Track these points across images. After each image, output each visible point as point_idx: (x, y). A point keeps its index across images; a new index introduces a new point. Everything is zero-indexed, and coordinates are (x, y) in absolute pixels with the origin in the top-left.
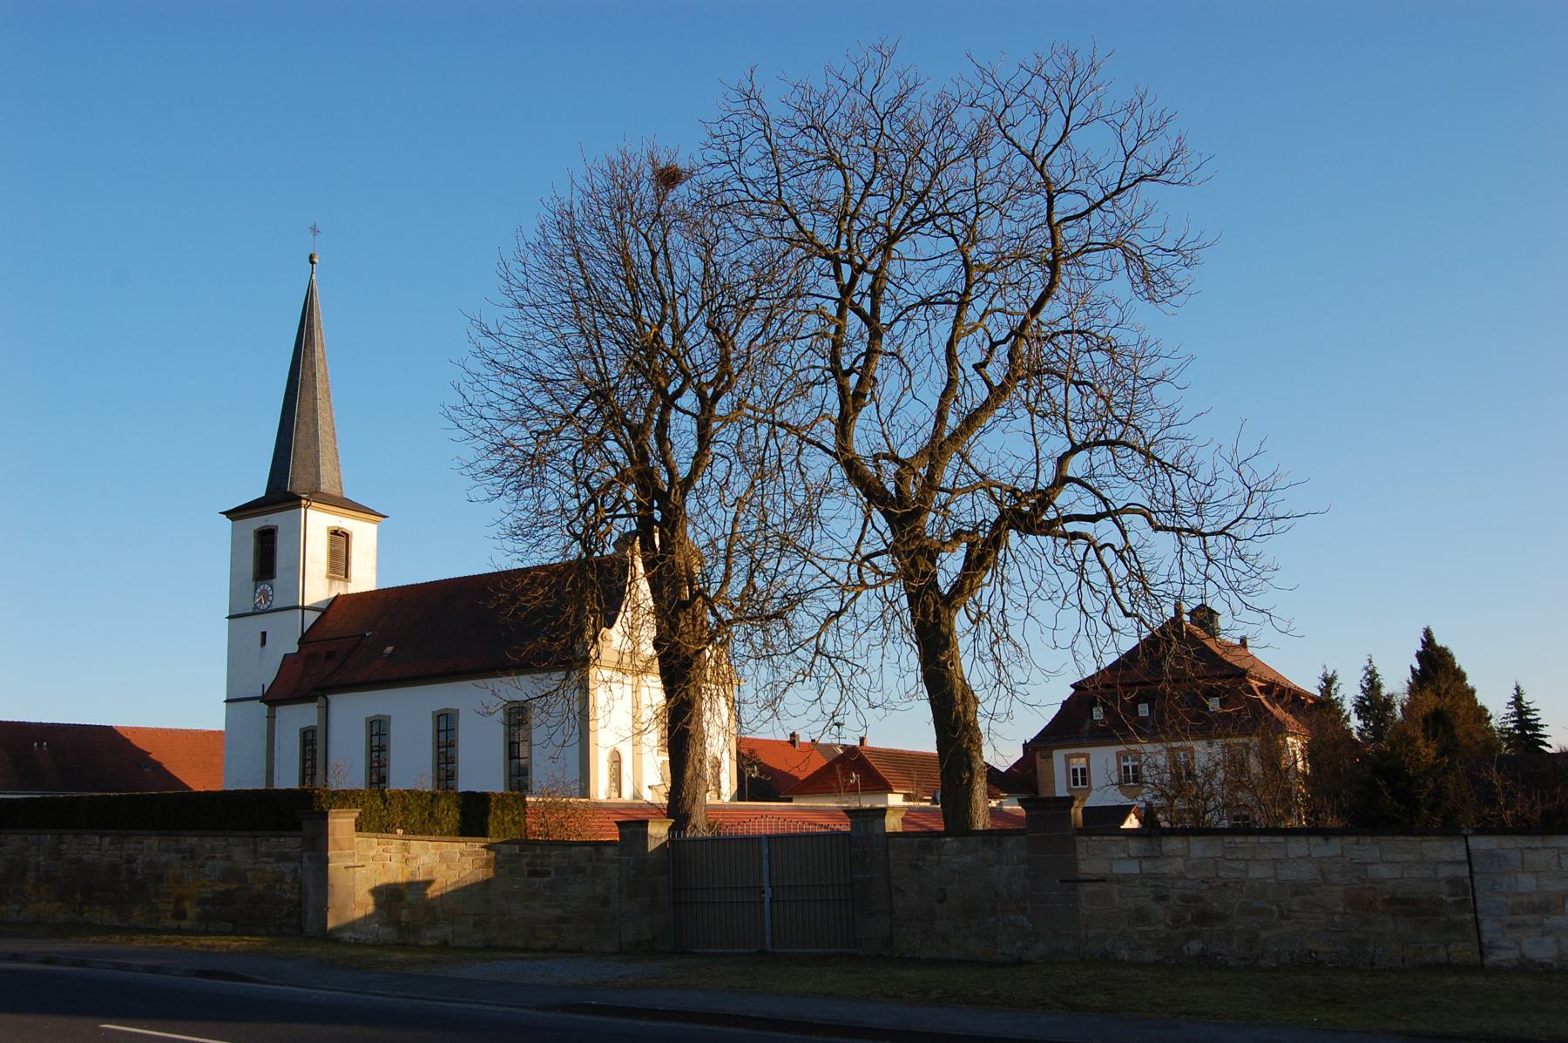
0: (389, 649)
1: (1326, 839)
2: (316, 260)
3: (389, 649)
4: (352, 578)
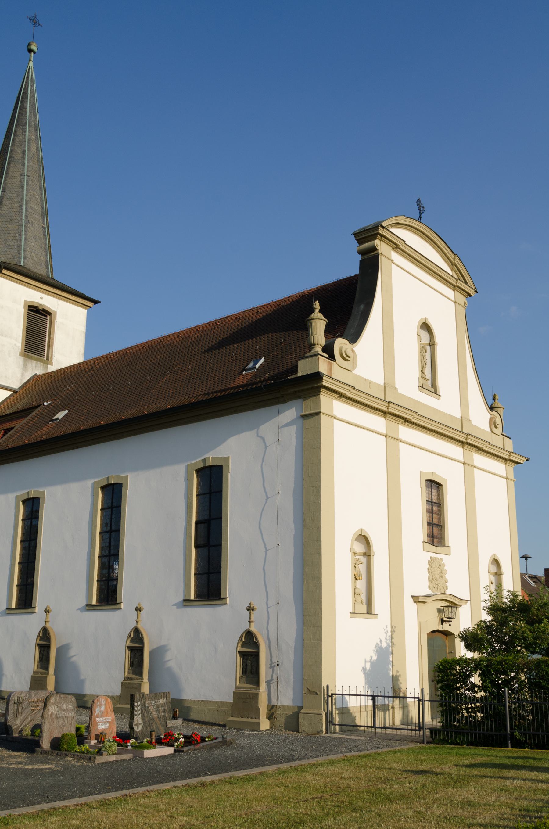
0: (61, 415)
1: (167, 651)
2: (34, 47)
3: (61, 415)
4: (54, 361)
